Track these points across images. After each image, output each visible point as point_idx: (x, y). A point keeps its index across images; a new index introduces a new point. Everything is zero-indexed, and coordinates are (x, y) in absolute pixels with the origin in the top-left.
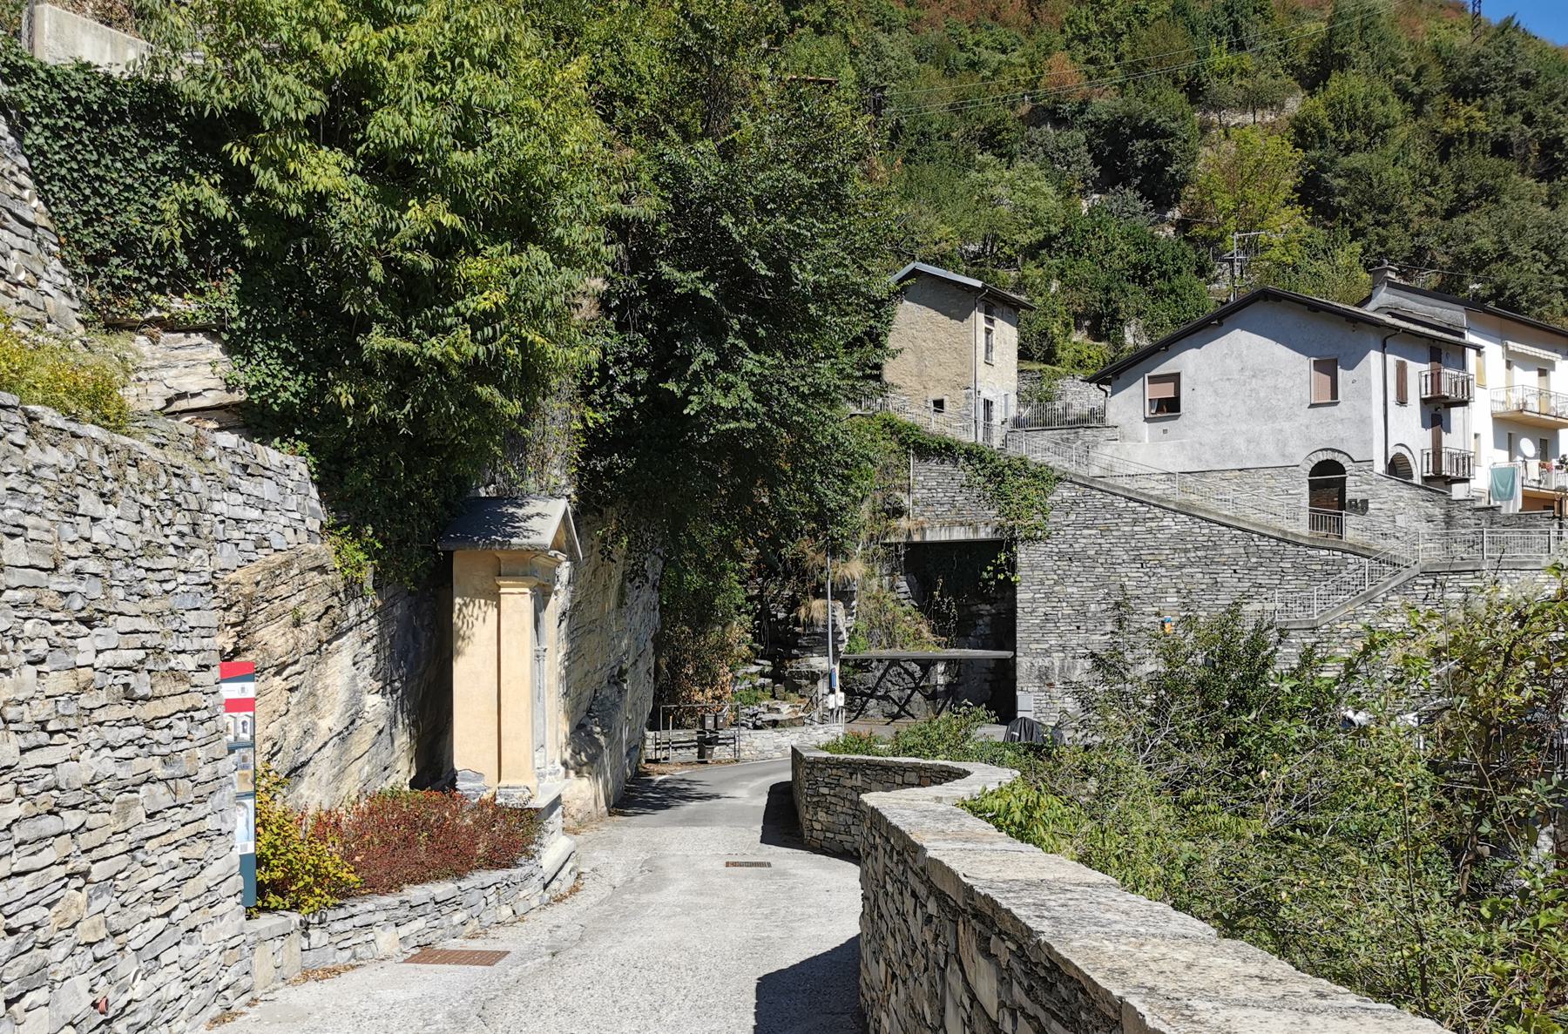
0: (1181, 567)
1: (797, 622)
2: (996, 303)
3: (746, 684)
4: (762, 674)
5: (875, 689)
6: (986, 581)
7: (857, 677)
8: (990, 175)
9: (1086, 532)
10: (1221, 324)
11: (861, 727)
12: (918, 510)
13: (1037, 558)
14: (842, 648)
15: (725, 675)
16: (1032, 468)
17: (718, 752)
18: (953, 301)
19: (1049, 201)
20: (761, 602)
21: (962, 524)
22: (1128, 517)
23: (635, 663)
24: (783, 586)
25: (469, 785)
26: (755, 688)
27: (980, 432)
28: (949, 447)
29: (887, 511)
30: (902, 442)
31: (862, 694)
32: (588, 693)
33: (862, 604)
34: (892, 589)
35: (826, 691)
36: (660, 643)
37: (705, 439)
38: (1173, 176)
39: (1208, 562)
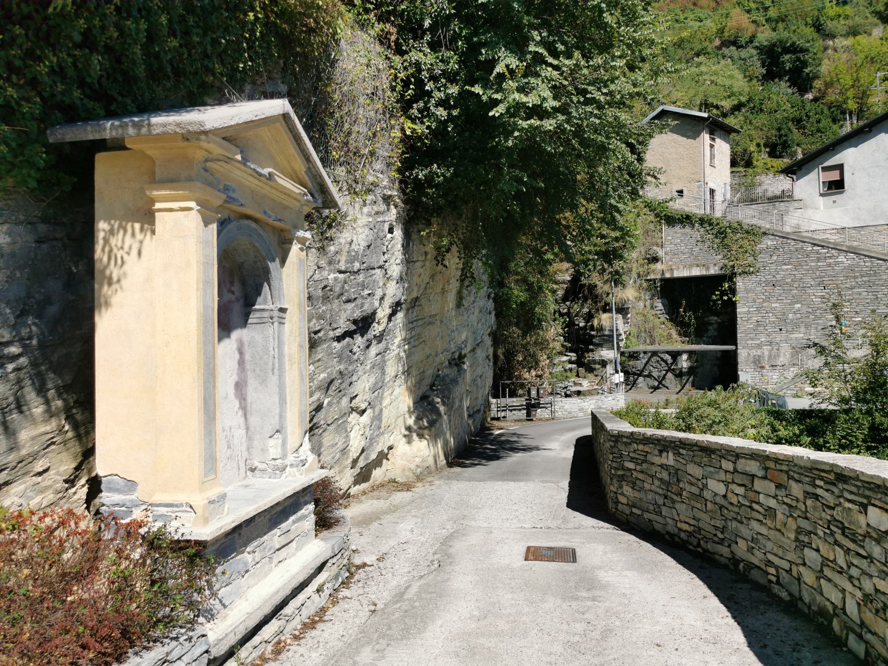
0: (852, 288)
1: (592, 328)
2: (717, 128)
3: (560, 368)
4: (570, 362)
5: (642, 371)
6: (715, 301)
7: (630, 363)
8: (703, 69)
9: (785, 267)
10: (870, 131)
11: (634, 395)
12: (668, 258)
13: (750, 285)
14: (622, 344)
15: (544, 361)
16: (746, 227)
17: (539, 413)
18: (689, 126)
19: (740, 83)
20: (569, 317)
21: (698, 266)
22: (814, 257)
23: (473, 350)
24: (582, 306)
25: (117, 498)
26: (566, 370)
27: (708, 207)
28: (688, 217)
29: (648, 259)
30: (657, 215)
31: (634, 374)
32: (430, 372)
33: (635, 318)
34: (652, 308)
35: (612, 372)
36: (497, 338)
37: (510, 143)
38: (808, 74)
39: (870, 285)
